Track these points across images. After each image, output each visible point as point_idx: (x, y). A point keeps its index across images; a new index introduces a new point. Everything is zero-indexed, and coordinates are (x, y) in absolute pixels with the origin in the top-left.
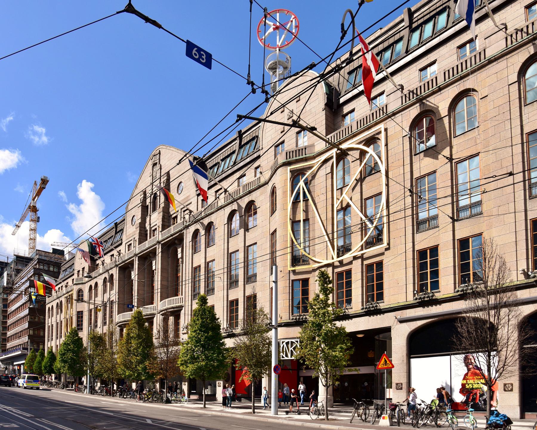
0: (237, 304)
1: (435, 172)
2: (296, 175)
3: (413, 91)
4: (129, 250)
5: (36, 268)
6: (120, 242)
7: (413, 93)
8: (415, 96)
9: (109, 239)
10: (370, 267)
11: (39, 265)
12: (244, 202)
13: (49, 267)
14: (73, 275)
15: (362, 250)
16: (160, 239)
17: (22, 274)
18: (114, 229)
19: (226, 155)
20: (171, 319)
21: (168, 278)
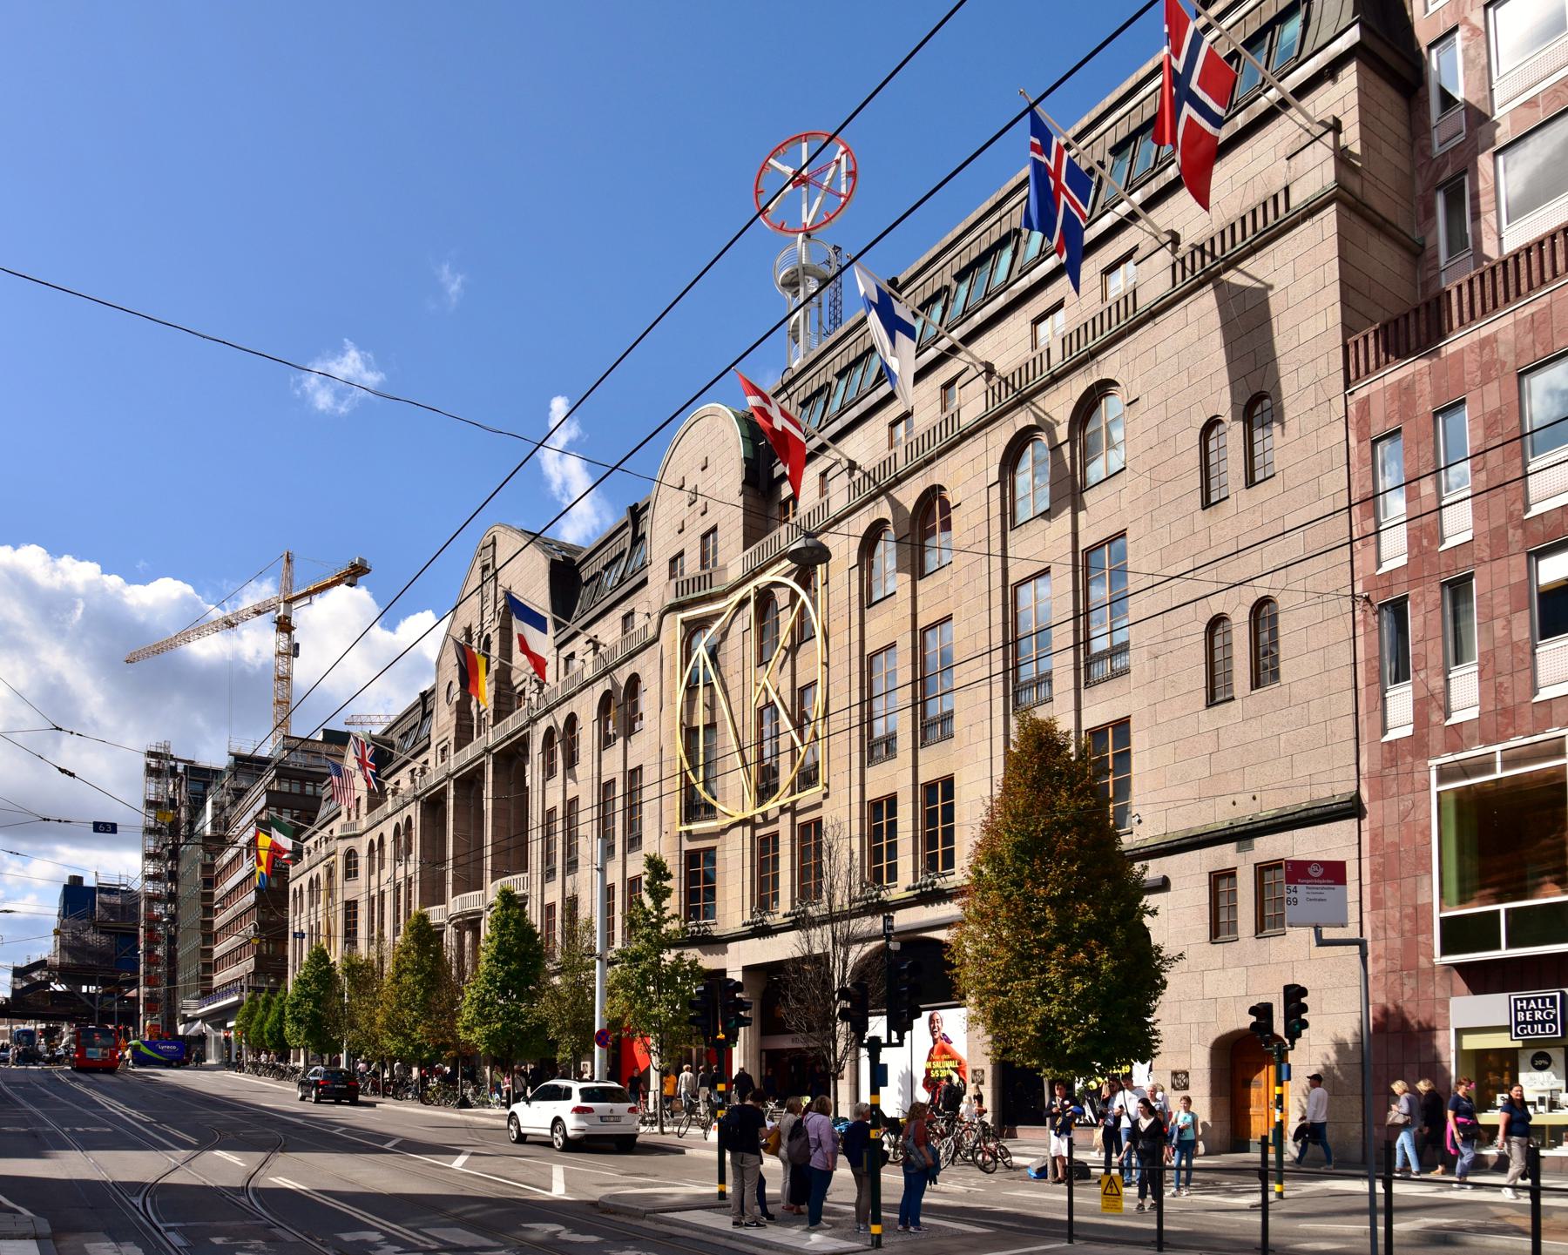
0: (893, 811)
1: (1122, 534)
2: (694, 628)
3: (1203, 245)
4: (566, 673)
5: (273, 791)
6: (426, 741)
7: (1203, 253)
8: (1208, 259)
9: (606, 568)
10: (805, 826)
11: (279, 784)
12: (909, 494)
13: (303, 787)
14: (339, 814)
15: (793, 793)
16: (491, 743)
17: (247, 800)
18: (421, 708)
19: (852, 358)
20: (468, 936)
21: (509, 829)
